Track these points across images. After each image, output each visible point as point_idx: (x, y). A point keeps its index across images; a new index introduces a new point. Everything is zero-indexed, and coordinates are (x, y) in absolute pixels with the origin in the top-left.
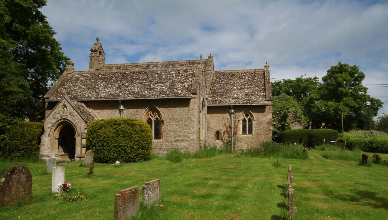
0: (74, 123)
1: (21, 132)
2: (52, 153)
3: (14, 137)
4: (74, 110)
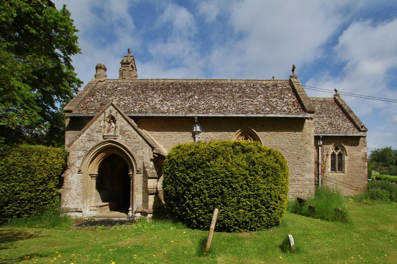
0: (130, 149)
1: (25, 165)
2: (85, 205)
3: (9, 175)
4: (130, 125)
